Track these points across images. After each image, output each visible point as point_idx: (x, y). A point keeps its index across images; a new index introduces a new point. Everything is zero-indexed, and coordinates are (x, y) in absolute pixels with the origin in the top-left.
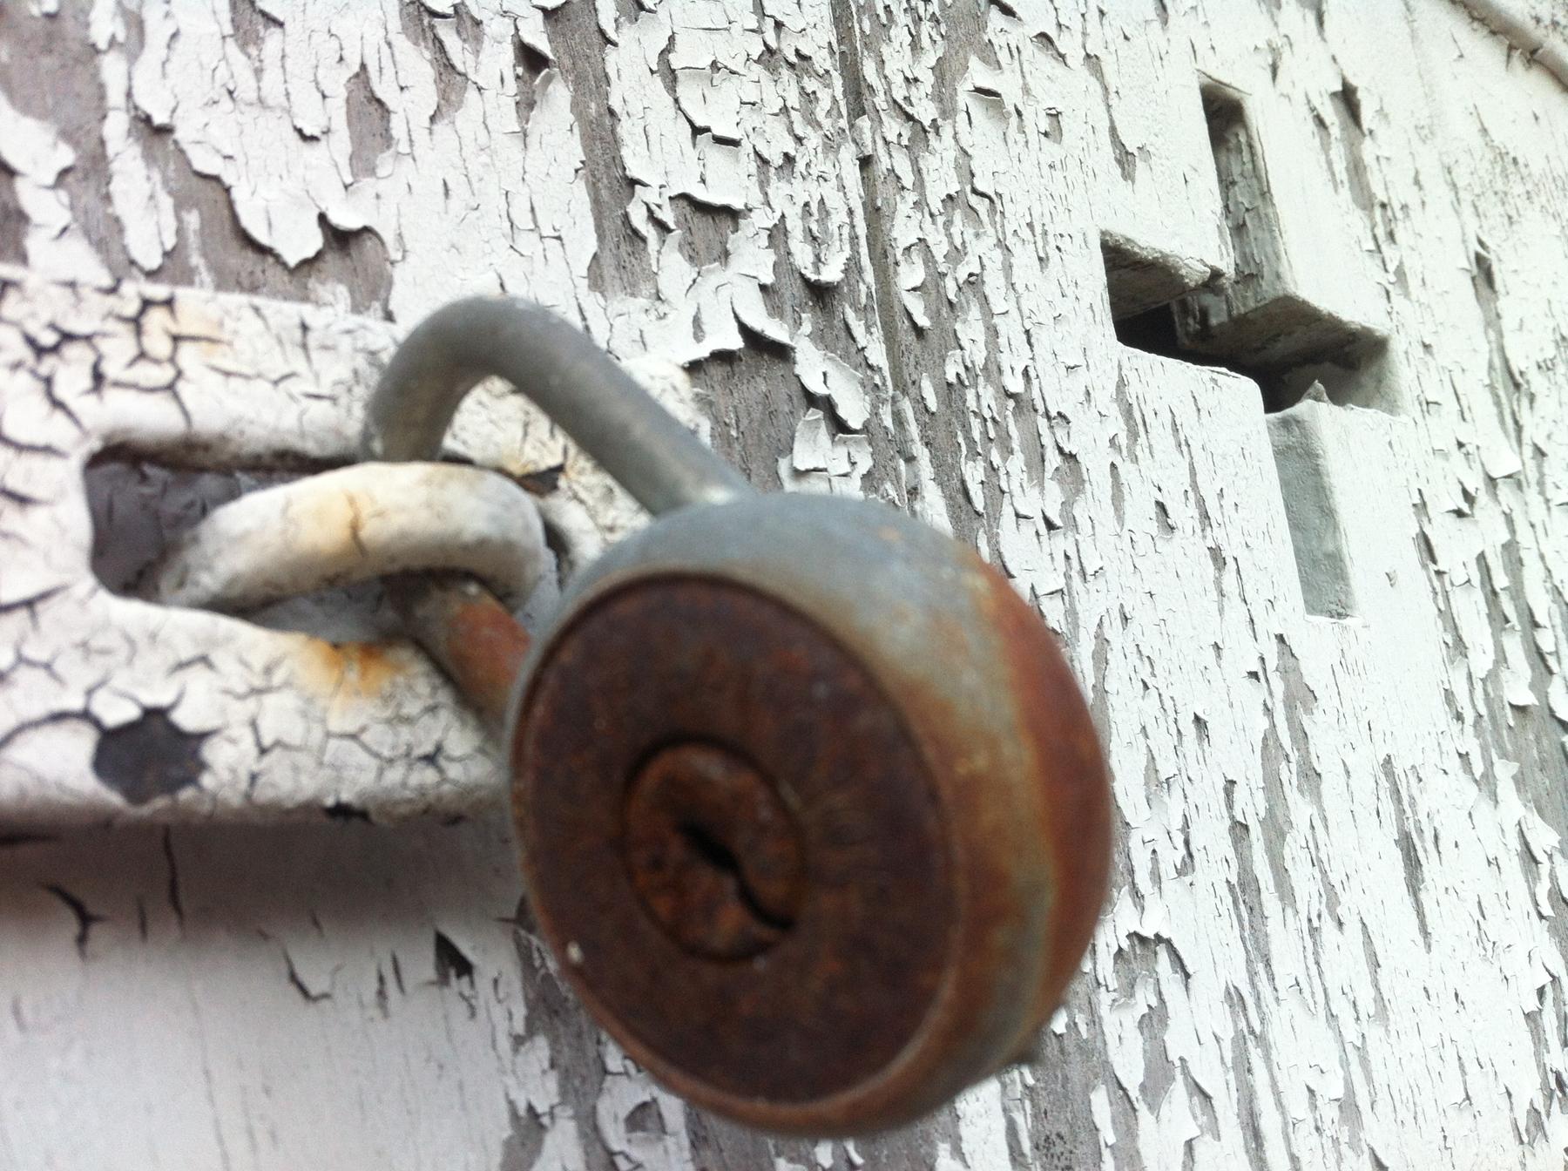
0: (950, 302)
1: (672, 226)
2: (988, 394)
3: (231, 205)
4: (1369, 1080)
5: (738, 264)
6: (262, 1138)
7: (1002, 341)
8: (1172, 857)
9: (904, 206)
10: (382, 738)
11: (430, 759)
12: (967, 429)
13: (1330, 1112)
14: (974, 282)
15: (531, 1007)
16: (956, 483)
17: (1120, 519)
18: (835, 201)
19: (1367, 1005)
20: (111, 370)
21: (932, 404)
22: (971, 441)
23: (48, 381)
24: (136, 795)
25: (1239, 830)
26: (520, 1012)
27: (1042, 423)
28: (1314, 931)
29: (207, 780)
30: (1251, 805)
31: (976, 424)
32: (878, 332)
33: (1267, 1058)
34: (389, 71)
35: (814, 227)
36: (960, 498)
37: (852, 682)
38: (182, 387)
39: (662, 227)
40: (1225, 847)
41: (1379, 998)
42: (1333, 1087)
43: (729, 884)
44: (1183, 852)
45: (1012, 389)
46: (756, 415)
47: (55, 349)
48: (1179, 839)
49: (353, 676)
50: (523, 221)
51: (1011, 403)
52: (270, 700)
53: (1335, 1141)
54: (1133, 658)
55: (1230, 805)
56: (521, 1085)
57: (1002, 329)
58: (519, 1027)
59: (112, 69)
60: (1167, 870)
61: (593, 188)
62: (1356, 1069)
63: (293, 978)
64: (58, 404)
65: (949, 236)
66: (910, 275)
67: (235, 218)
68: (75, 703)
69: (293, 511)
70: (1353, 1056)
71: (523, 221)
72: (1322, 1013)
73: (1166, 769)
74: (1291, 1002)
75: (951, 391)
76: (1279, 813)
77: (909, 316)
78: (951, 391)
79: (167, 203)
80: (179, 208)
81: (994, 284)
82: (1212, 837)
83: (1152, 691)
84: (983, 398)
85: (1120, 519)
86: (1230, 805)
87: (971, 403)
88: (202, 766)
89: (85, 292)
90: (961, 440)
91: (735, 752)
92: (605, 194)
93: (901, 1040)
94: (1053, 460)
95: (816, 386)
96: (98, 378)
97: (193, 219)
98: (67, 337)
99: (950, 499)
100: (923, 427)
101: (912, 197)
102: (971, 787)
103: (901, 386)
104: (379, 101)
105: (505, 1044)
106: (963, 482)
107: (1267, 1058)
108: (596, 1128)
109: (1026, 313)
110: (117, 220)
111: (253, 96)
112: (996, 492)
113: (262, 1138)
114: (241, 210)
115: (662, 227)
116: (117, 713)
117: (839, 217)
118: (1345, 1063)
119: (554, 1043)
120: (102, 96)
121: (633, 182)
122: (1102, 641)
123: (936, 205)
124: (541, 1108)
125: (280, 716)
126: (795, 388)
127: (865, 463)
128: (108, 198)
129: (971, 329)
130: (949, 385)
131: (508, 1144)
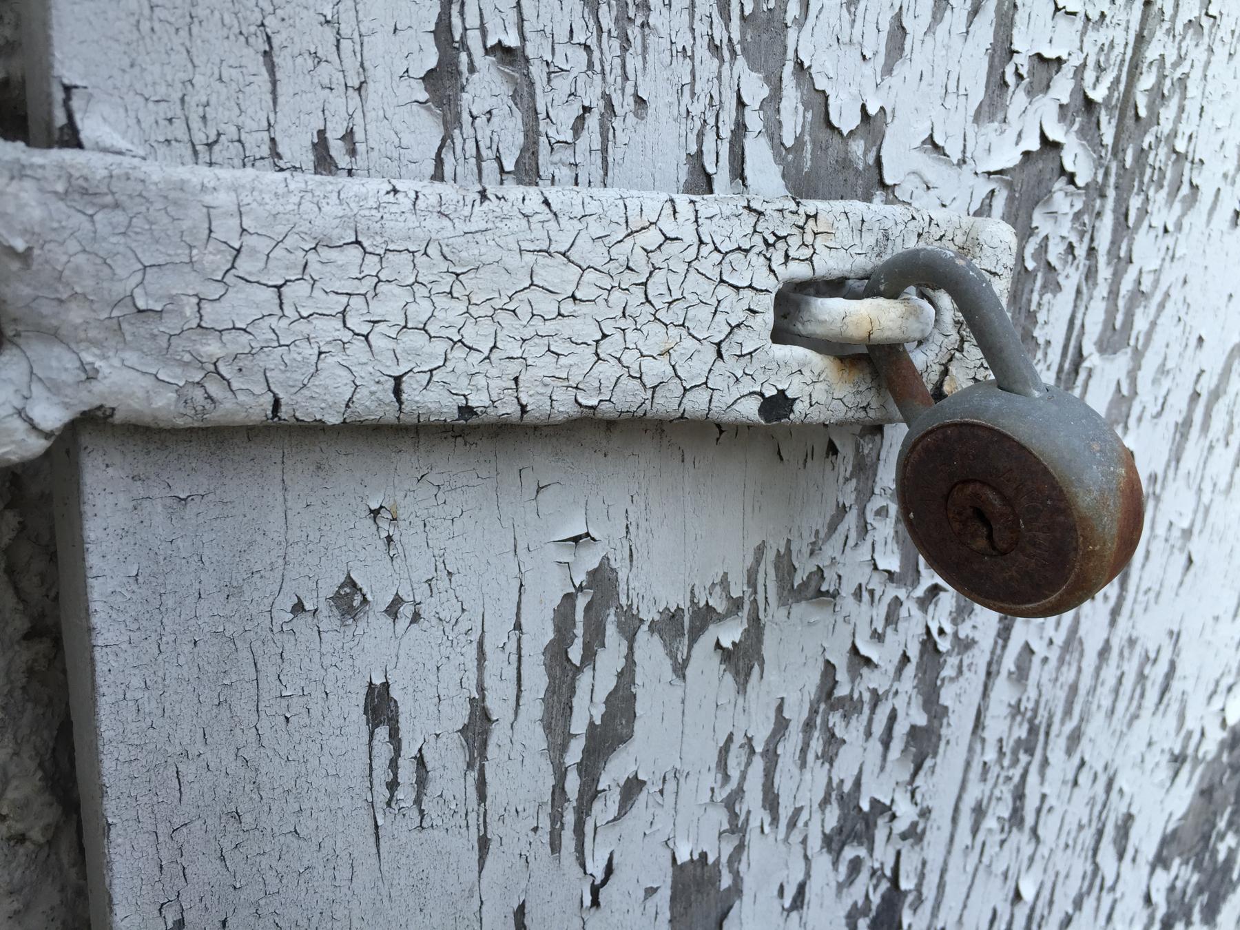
0: (1163, 95)
1: (1025, 75)
2: (1163, 151)
3: (827, 105)
4: (1205, 520)
5: (1053, 93)
6: (757, 508)
7: (1184, 116)
8: (1153, 409)
9: (1160, 34)
10: (850, 400)
11: (864, 408)
12: (1142, 174)
13: (1176, 533)
14: (1183, 81)
15: (854, 467)
16: (1123, 210)
17: (1209, 222)
18: (1119, 42)
19: (1222, 484)
20: (792, 253)
21: (1128, 164)
22: (1141, 182)
23: (769, 260)
24: (767, 420)
25: (1196, 395)
26: (850, 469)
27: (1188, 165)
28: (1211, 447)
29: (792, 416)
30: (1205, 387)
31: (1148, 171)
32: (1114, 122)
33: (1156, 507)
34: (911, 9)
35: (1102, 59)
36: (1122, 218)
37: (1062, 505)
38: (815, 258)
39: (1019, 77)
40: (1184, 405)
41: (1230, 485)
42: (1185, 524)
43: (984, 531)
44: (1159, 408)
45: (1178, 149)
46: (1032, 183)
47: (773, 245)
48: (1160, 401)
49: (845, 375)
50: (952, 88)
51: (1174, 157)
52: (818, 386)
53: (1173, 547)
54: (1180, 304)
55: (1197, 381)
56: (843, 495)
57: (1187, 109)
58: (848, 475)
59: (792, 34)
60: (1147, 415)
61: (992, 58)
62: (1200, 515)
63: (779, 453)
64: (772, 270)
65: (1180, 48)
66: (1147, 81)
67: (827, 114)
68: (758, 389)
69: (847, 320)
70: (1201, 509)
71: (952, 88)
72: (1195, 487)
73: (1170, 365)
74: (1181, 482)
75: (1141, 154)
76: (1221, 387)
77: (1136, 108)
78: (1141, 154)
79: (801, 108)
80: (806, 110)
81: (1193, 90)
82: (1179, 402)
83: (1182, 323)
84: (1160, 157)
85: (1209, 222)
86: (1197, 381)
87: (1151, 160)
88: (792, 411)
89: (786, 213)
90: (1136, 184)
91: (1006, 500)
92: (997, 60)
93: (1030, 601)
94: (1185, 189)
95: (1069, 167)
96: (787, 256)
97: (809, 115)
98: (779, 238)
99: (1116, 219)
100: (1118, 176)
101: (1166, 25)
102: (1089, 555)
103: (1115, 153)
104: (903, 28)
105: (841, 480)
106: (1127, 210)
107: (1156, 507)
108: (864, 513)
109: (1207, 93)
110: (780, 122)
111: (847, 39)
112: (1144, 212)
113: (757, 508)
114: (831, 109)
115: (1019, 77)
116: (770, 392)
117: (1119, 49)
118: (1196, 512)
119: (858, 481)
120: (785, 53)
121: (1012, 52)
122: (1167, 295)
123: (1179, 27)
124: (847, 505)
125: (819, 394)
126: (1058, 164)
127: (1079, 205)
128: (778, 111)
129: (1167, 114)
130: (1142, 150)
131: (833, 516)
